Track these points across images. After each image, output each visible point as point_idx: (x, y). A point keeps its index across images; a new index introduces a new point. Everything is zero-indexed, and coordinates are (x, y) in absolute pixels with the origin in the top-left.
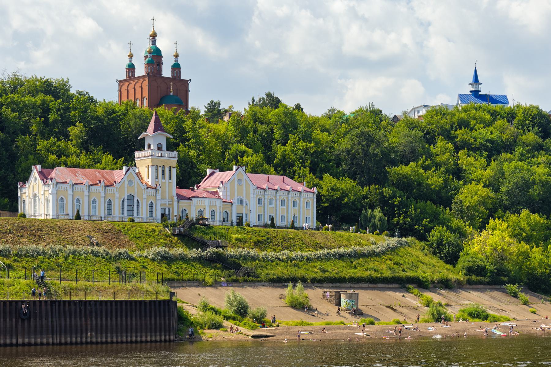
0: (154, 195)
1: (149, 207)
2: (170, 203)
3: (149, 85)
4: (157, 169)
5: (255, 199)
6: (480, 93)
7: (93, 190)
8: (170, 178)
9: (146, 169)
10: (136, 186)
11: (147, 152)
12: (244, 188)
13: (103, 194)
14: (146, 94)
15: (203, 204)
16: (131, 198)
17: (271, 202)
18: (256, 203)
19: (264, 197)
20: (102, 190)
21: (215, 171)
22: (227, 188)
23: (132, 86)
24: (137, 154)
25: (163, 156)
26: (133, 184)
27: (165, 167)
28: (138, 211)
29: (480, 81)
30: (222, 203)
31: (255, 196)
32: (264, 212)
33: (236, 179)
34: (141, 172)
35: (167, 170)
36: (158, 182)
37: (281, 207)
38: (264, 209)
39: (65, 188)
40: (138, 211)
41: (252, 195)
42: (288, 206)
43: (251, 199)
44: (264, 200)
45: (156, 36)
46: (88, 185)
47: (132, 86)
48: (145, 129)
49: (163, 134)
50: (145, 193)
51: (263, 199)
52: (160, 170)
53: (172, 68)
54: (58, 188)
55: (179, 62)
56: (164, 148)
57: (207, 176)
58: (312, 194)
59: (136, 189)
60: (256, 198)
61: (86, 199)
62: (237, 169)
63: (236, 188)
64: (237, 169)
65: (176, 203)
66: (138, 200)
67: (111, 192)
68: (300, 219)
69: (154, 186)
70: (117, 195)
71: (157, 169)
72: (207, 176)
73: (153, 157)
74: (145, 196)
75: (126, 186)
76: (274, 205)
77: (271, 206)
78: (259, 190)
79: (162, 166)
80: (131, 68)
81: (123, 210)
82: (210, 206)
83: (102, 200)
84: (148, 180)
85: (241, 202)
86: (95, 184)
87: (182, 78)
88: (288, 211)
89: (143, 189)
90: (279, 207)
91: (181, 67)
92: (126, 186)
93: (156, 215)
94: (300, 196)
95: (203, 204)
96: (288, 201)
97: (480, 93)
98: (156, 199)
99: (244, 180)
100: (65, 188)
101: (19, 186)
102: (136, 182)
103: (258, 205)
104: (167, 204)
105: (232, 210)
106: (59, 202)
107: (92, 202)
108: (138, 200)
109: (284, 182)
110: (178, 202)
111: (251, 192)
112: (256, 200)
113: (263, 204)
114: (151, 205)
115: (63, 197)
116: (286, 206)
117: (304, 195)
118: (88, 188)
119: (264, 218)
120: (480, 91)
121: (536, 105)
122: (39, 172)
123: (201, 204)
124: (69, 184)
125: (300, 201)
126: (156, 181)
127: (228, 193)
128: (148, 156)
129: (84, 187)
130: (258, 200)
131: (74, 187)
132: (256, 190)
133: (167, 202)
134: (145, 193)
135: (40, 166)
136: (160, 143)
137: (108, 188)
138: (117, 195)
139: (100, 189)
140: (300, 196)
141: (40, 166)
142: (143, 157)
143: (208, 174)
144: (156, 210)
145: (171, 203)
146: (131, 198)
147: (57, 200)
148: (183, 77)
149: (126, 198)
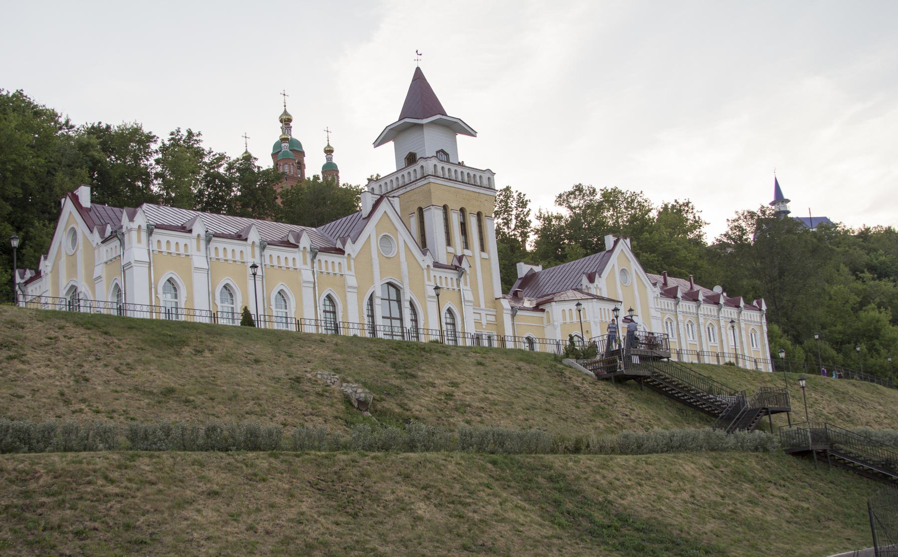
0: (455, 287)
6: (789, 215)
8: (483, 249)
26: (395, 250)
27: (467, 214)
29: (786, 197)
42: (722, 341)
44: (678, 324)
45: (290, 120)
46: (257, 242)
50: (429, 279)
52: (455, 219)
55: (334, 161)
89: (424, 266)
91: (339, 168)
97: (789, 215)
101: (18, 280)
102: (402, 244)
111: (652, 303)
115: (174, 277)
120: (789, 212)
123: (568, 320)
131: (213, 245)
134: (429, 279)
138: (352, 281)
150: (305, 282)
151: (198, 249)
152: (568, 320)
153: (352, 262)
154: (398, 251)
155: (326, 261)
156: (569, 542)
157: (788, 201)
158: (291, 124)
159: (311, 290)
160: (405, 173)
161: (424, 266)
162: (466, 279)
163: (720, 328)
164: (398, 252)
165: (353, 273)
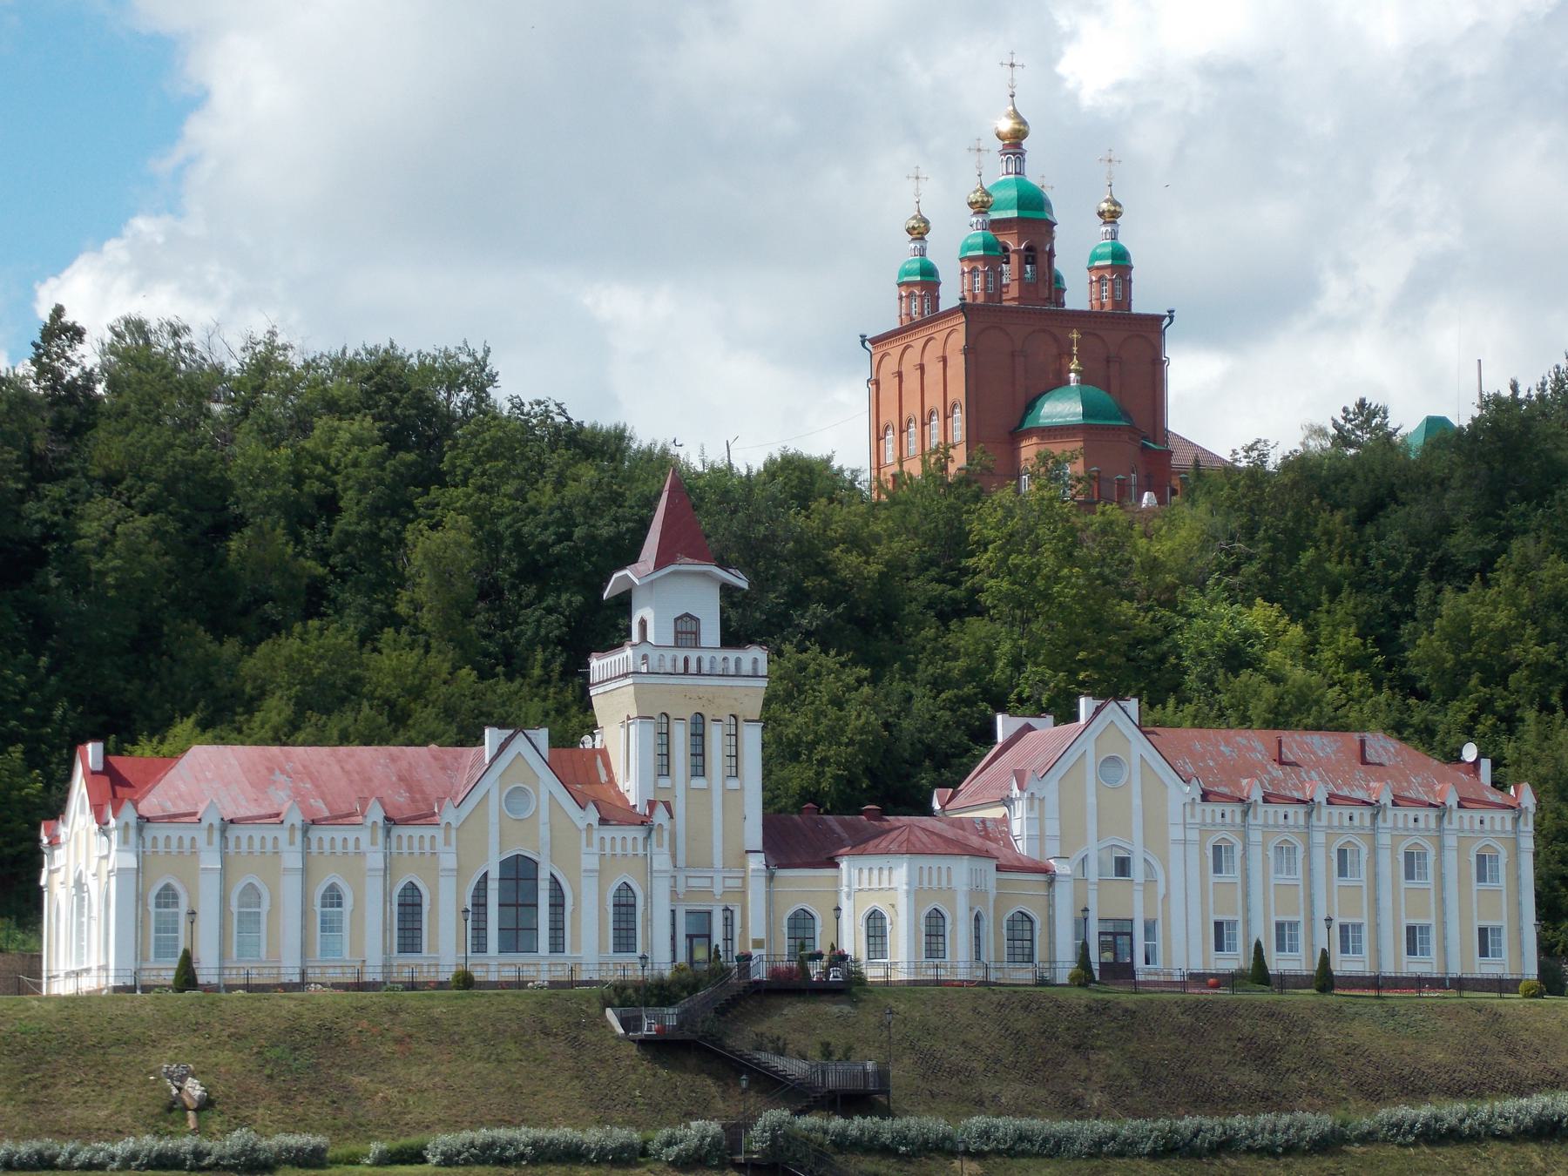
0: (640, 851)
1: (611, 909)
2: (729, 883)
3: (969, 351)
4: (665, 738)
5: (1194, 852)
7: (327, 846)
9: (623, 732)
10: (544, 815)
11: (624, 657)
12: (1137, 801)
13: (376, 860)
14: (958, 391)
15: (944, 884)
16: (519, 872)
17: (1412, 864)
18: (1329, 869)
19: (1245, 838)
20: (373, 843)
21: (1033, 721)
22: (1042, 800)
23: (912, 357)
24: (599, 665)
25: (706, 668)
28: (557, 928)
30: (992, 875)
31: (1194, 835)
32: (1247, 909)
33: (1091, 762)
34: (610, 750)
35: (716, 737)
36: (671, 789)
37: (1337, 882)
38: (1246, 895)
39: (187, 843)
40: (557, 928)
41: (1176, 833)
43: (1176, 852)
46: (298, 824)
47: (912, 357)
48: (630, 555)
49: (704, 574)
50: (589, 844)
51: (1364, 852)
52: (680, 736)
53: (1059, 279)
54: (149, 843)
56: (711, 632)
57: (996, 748)
58: (1508, 816)
59: (544, 832)
60: (1202, 843)
61: (291, 888)
62: (1098, 710)
63: (1091, 800)
64: (1098, 710)
65: (757, 890)
66: (554, 881)
67: (416, 850)
68: (1445, 938)
69: (642, 809)
70: (448, 860)
71: (665, 738)
72: (996, 748)
73: (640, 679)
74: (590, 861)
75: (493, 817)
76: (1300, 874)
77: (1284, 878)
78: (1216, 808)
79: (688, 715)
80: (927, 280)
81: (480, 931)
82: (917, 893)
83: (374, 890)
84: (627, 784)
85: (1123, 866)
86: (337, 819)
87: (1137, 308)
88: (1375, 902)
89: (582, 825)
90: (1395, 885)
92: (493, 817)
93: (649, 944)
94: (1308, 826)
95: (944, 884)
96: (1374, 851)
98: (649, 872)
99: (1136, 761)
100: (187, 843)
102: (544, 798)
103: (1212, 878)
104: (718, 889)
105: (1051, 905)
106: (152, 908)
107: (318, 901)
108: (554, 881)
109: (1364, 761)
110: (771, 878)
112: (1202, 855)
113: (1238, 872)
114: (624, 908)
116: (1364, 876)
117: (1462, 820)
118: (298, 836)
119: (1443, 937)
121: (1328, 412)
122: (94, 773)
123: (935, 882)
124: (205, 824)
125: (1441, 849)
126: (657, 789)
127: (1053, 828)
128: (626, 675)
129: (283, 835)
130: (1402, 859)
132: (1200, 807)
133: (718, 878)
134: (589, 844)
135: (100, 745)
136: (687, 615)
137: (404, 831)
139: (365, 836)
140: (1308, 826)
141: (100, 745)
142: (611, 679)
143: (1000, 738)
144: (648, 921)
145: (738, 883)
146: (519, 872)
147: (141, 898)
148: (1139, 306)
149: (494, 874)
150: (370, 870)
151: (210, 843)
152: (926, 885)
153: (453, 833)
154: (537, 807)
155: (411, 837)
156: (548, 1072)
158: (1119, 220)
159: (382, 879)
160: (669, 654)
161: (582, 825)
162: (1526, 818)
163: (1374, 851)
164: (1128, 782)
165: (453, 849)
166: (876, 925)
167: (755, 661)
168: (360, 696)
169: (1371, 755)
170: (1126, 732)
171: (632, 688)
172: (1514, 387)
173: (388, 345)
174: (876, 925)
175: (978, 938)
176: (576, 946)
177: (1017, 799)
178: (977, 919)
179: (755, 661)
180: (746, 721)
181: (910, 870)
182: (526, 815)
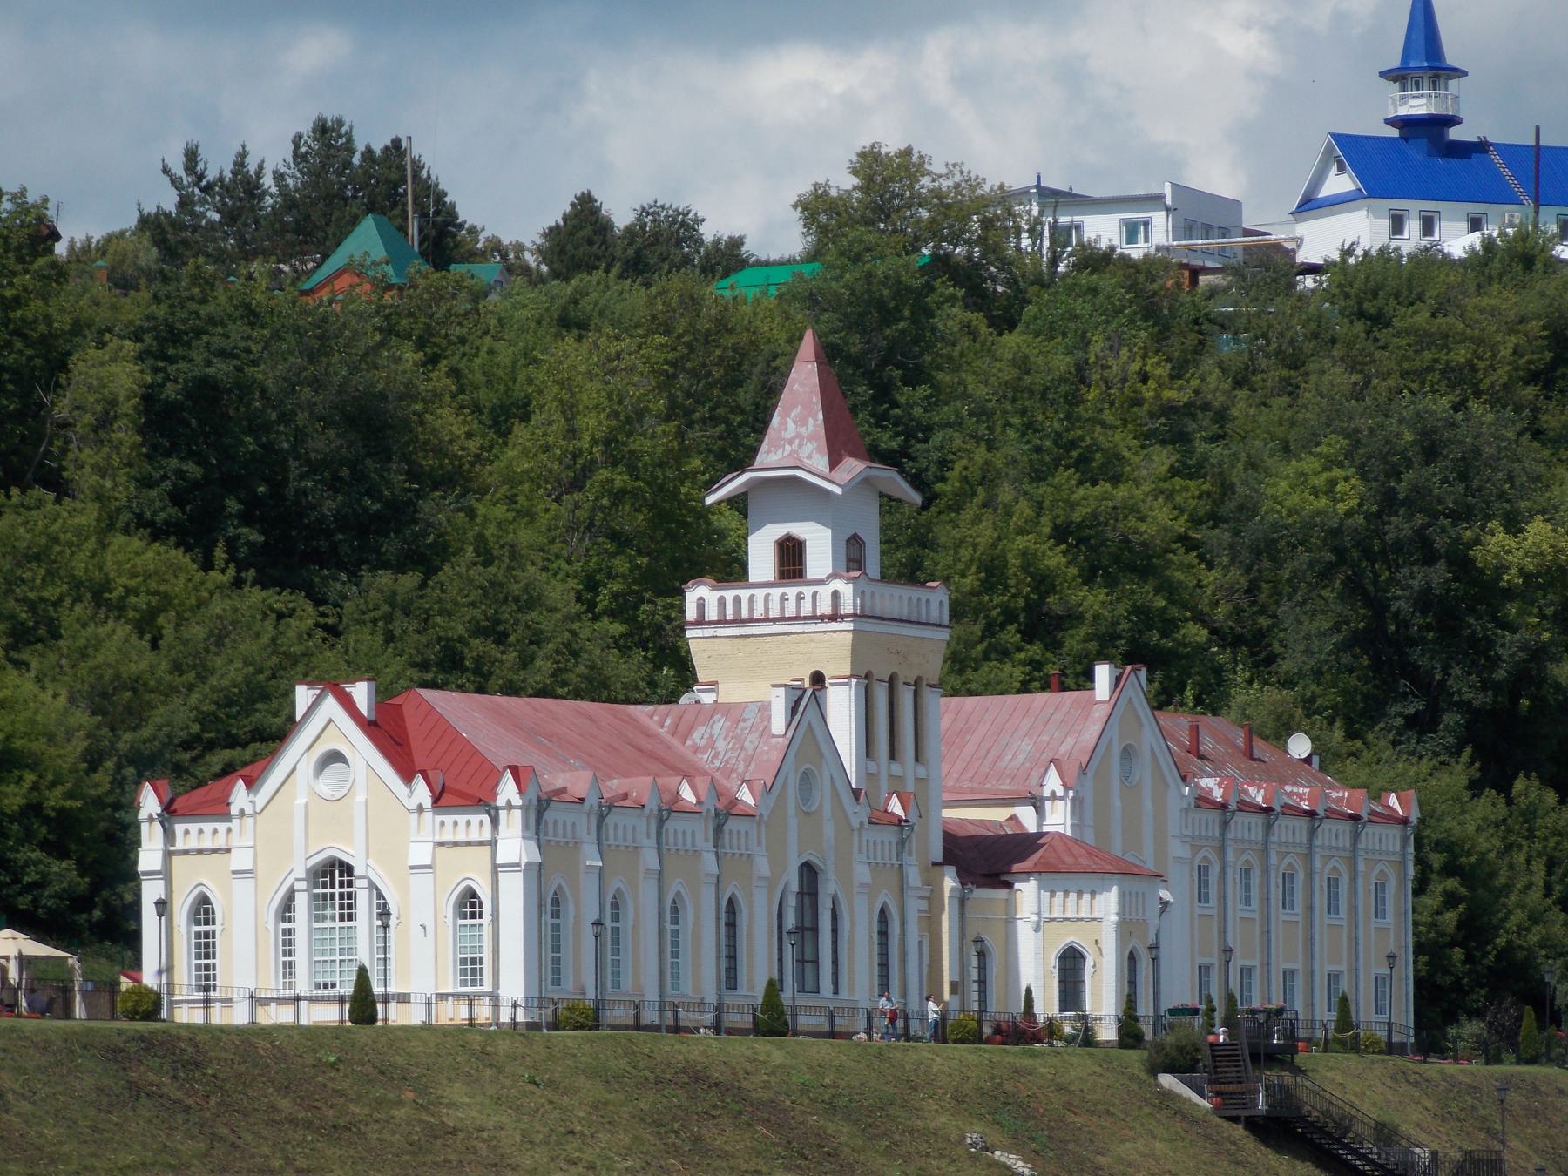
37: (1373, 922)
82: (1126, 927)
115: (468, 882)
124: (646, 810)
157: (1458, 73)
159: (713, 888)
166: (1071, 964)
167: (835, 595)
168: (961, 672)
169: (1256, 754)
170: (1142, 714)
171: (850, 636)
172: (851, 161)
173: (1093, 237)
174: (1071, 964)
175: (732, 958)
176: (851, 989)
177: (1053, 797)
178: (1132, 958)
179: (835, 595)
180: (928, 685)
181: (1123, 896)
182: (814, 808)
